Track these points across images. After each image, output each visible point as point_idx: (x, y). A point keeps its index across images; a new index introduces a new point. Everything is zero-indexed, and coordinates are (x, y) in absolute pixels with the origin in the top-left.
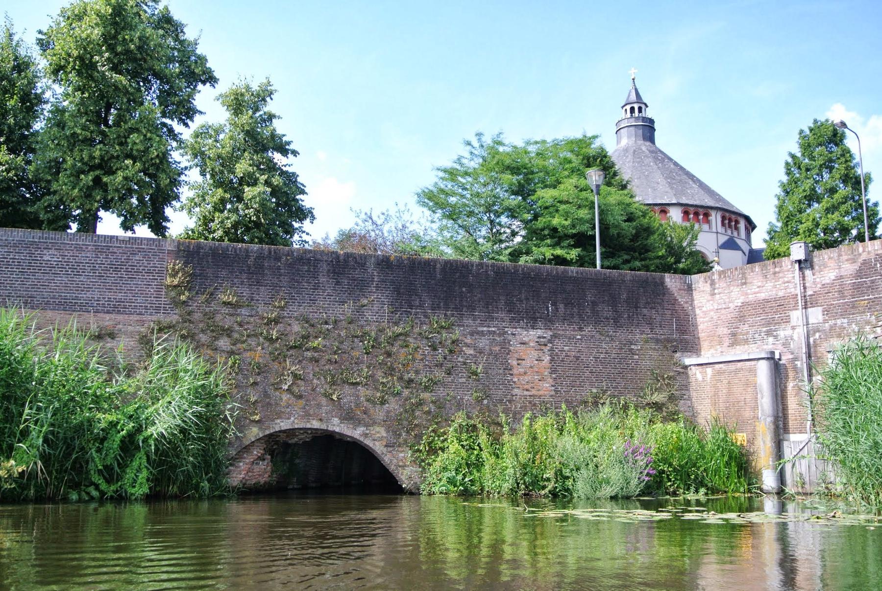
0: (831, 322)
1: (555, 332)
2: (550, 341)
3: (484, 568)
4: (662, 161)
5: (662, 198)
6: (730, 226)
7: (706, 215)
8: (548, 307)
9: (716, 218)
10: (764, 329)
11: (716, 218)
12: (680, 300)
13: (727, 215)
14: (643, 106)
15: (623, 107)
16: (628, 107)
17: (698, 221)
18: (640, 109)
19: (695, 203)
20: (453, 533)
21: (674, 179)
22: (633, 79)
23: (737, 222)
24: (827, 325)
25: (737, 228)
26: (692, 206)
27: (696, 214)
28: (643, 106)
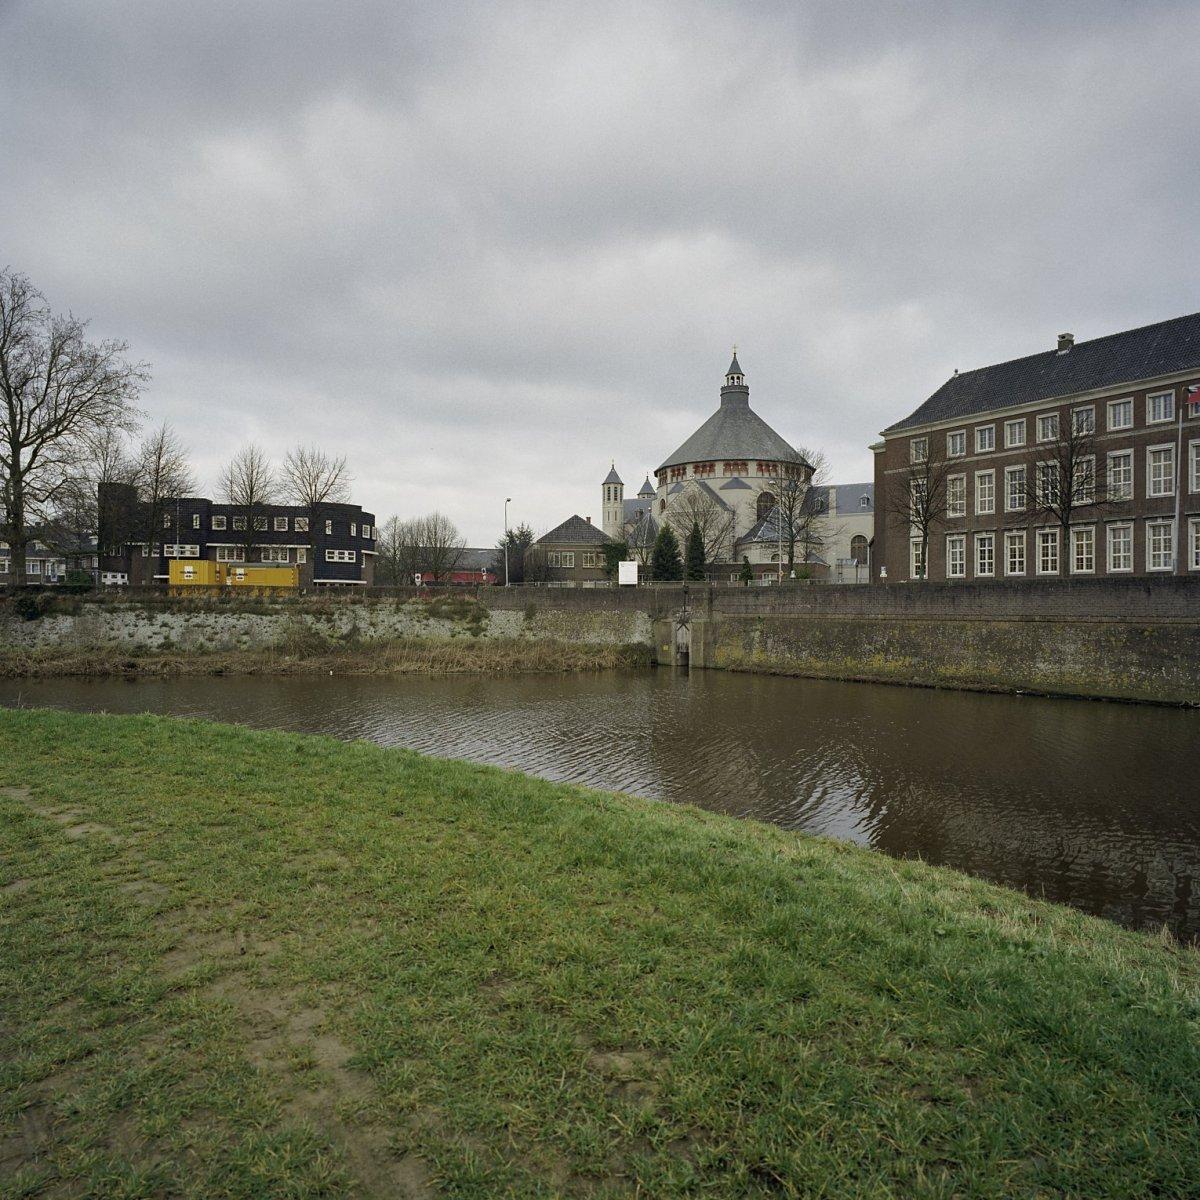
7: (775, 466)
14: (741, 376)
16: (730, 377)
18: (738, 378)
19: (767, 458)
23: (798, 469)
27: (768, 466)
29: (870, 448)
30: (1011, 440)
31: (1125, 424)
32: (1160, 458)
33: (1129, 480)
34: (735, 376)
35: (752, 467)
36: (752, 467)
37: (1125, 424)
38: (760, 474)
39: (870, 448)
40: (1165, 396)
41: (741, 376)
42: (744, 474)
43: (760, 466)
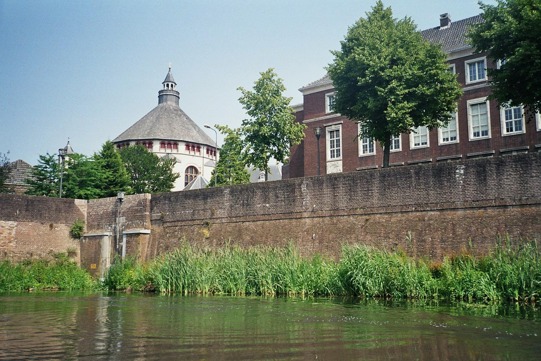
0: (128, 223)
1: (19, 222)
2: (16, 226)
3: (98, 340)
4: (180, 116)
5: (175, 137)
6: (211, 154)
7: (199, 148)
8: (17, 212)
9: (203, 150)
10: (108, 224)
11: (203, 150)
12: (81, 210)
13: (210, 148)
15: (163, 83)
16: (166, 84)
17: (194, 150)
18: (172, 86)
19: (193, 141)
20: (118, 323)
21: (184, 127)
22: (170, 68)
23: (215, 152)
24: (126, 224)
25: (215, 155)
26: (191, 142)
28: (174, 85)
29: (301, 90)
30: (471, 77)
31: (479, 79)
32: (334, 136)
33: (366, 142)
34: (170, 84)
35: (182, 147)
36: (182, 147)
37: (479, 79)
38: (187, 152)
39: (301, 90)
40: (479, 62)
41: (174, 84)
42: (175, 151)
43: (208, 150)
